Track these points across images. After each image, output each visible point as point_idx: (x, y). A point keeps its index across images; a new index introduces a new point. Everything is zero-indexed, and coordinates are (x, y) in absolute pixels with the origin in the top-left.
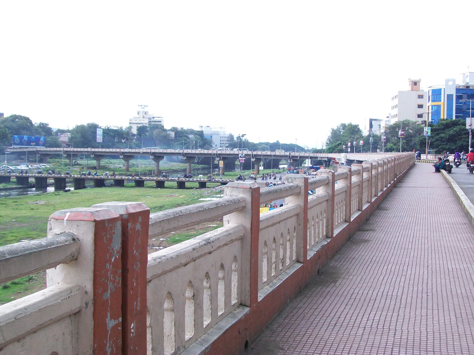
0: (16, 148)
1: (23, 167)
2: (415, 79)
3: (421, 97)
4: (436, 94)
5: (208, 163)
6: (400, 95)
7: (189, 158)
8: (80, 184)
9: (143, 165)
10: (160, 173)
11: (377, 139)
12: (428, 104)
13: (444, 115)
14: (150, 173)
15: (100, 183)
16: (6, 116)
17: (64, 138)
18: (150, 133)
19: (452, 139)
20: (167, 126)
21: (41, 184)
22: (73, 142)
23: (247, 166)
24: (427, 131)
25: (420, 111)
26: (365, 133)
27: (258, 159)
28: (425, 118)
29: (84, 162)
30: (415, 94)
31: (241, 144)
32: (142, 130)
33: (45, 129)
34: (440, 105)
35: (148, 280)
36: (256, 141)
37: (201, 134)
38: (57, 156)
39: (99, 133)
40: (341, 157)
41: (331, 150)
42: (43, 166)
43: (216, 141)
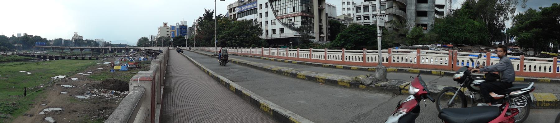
0: (36, 46)
1: (39, 52)
2: (165, 22)
3: (168, 29)
4: (173, 27)
5: (98, 51)
6: (161, 28)
7: (92, 50)
8: (57, 58)
9: (76, 52)
10: (82, 55)
11: (154, 42)
12: (170, 31)
13: (176, 35)
14: (79, 55)
15: (63, 58)
16: (190, 25)
17: (51, 43)
18: (78, 41)
19: (180, 42)
20: (84, 39)
21: (45, 58)
22: (54, 44)
23: (112, 52)
24: (172, 40)
25: (168, 33)
26: (150, 40)
27: (115, 49)
28: (170, 35)
29: (58, 51)
30: (166, 28)
31: (109, 44)
32: (76, 40)
33: (45, 39)
34: (369, 19)
35: (413, 80)
36: (114, 44)
37: (95, 42)
38: (49, 49)
39: (63, 41)
40: (143, 49)
41: (139, 46)
42: (45, 52)
43: (101, 44)
